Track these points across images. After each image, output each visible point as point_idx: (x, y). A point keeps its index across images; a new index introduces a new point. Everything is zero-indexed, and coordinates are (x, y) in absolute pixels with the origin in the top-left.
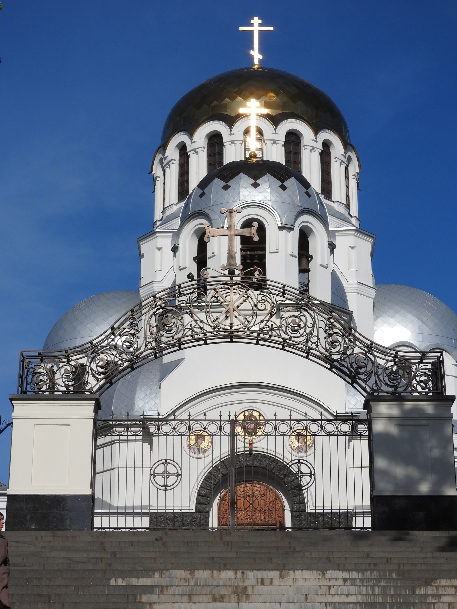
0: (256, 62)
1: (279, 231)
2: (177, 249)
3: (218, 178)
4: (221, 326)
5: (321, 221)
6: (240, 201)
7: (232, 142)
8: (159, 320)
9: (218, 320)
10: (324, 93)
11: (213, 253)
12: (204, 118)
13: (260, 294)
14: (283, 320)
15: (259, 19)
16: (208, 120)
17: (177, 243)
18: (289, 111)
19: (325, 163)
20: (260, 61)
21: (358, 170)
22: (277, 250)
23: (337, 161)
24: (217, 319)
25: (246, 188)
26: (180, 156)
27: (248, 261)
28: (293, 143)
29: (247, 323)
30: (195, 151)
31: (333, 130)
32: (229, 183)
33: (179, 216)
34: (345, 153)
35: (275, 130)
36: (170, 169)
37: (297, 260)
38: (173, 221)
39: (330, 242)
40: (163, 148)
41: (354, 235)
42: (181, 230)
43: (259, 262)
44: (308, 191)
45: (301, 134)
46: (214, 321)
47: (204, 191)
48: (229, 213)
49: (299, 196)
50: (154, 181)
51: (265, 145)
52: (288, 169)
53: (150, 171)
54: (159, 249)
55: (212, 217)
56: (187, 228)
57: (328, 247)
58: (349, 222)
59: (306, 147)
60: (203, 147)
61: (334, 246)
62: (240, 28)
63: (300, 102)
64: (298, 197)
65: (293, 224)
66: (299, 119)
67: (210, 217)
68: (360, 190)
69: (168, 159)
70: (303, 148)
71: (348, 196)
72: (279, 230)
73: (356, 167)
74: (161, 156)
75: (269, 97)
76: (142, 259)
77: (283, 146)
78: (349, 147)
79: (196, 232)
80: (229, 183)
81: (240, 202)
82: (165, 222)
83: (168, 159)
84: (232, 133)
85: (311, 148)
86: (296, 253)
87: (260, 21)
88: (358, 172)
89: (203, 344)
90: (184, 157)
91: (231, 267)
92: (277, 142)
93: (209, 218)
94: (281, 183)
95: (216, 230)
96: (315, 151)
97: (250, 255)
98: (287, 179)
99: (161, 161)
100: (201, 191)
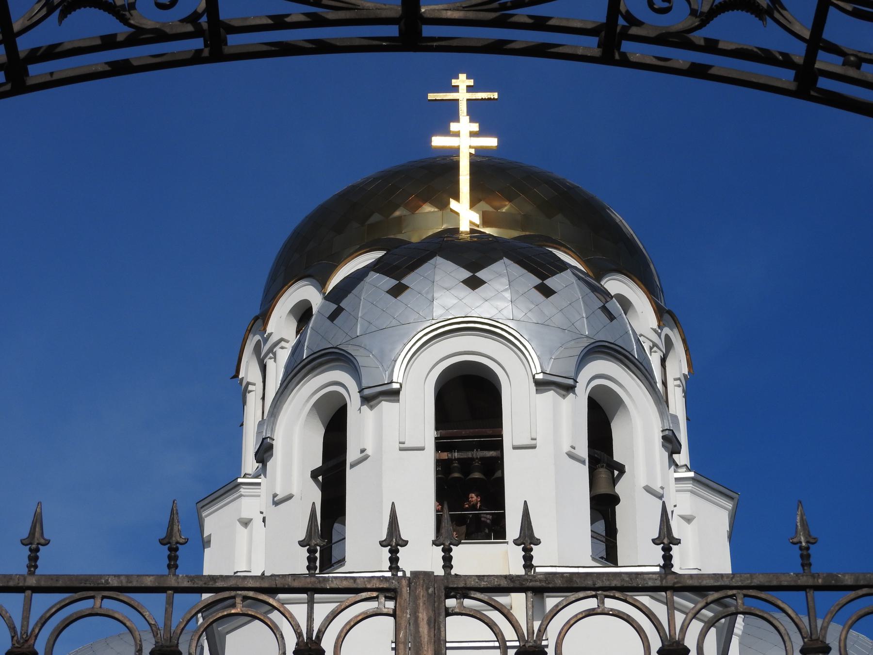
1: (536, 393)
5: (643, 378)
11: (363, 451)
18: (537, 234)
22: (532, 439)
25: (448, 289)
27: (456, 475)
32: (405, 281)
34: (659, 326)
36: (275, 361)
37: (585, 470)
39: (667, 433)
41: (692, 492)
42: (280, 402)
43: (484, 477)
49: (586, 312)
50: (243, 393)
53: (234, 373)
54: (246, 523)
55: (361, 361)
57: (663, 446)
65: (572, 375)
66: (559, 247)
67: (355, 362)
68: (689, 420)
69: (274, 339)
72: (538, 391)
74: (258, 337)
76: (205, 550)
78: (667, 317)
79: (319, 406)
80: (405, 281)
83: (274, 339)
86: (583, 451)
87: (471, 82)
89: (196, 59)
94: (538, 281)
97: (459, 460)
98: (554, 274)
99: (257, 349)
100: (334, 307)
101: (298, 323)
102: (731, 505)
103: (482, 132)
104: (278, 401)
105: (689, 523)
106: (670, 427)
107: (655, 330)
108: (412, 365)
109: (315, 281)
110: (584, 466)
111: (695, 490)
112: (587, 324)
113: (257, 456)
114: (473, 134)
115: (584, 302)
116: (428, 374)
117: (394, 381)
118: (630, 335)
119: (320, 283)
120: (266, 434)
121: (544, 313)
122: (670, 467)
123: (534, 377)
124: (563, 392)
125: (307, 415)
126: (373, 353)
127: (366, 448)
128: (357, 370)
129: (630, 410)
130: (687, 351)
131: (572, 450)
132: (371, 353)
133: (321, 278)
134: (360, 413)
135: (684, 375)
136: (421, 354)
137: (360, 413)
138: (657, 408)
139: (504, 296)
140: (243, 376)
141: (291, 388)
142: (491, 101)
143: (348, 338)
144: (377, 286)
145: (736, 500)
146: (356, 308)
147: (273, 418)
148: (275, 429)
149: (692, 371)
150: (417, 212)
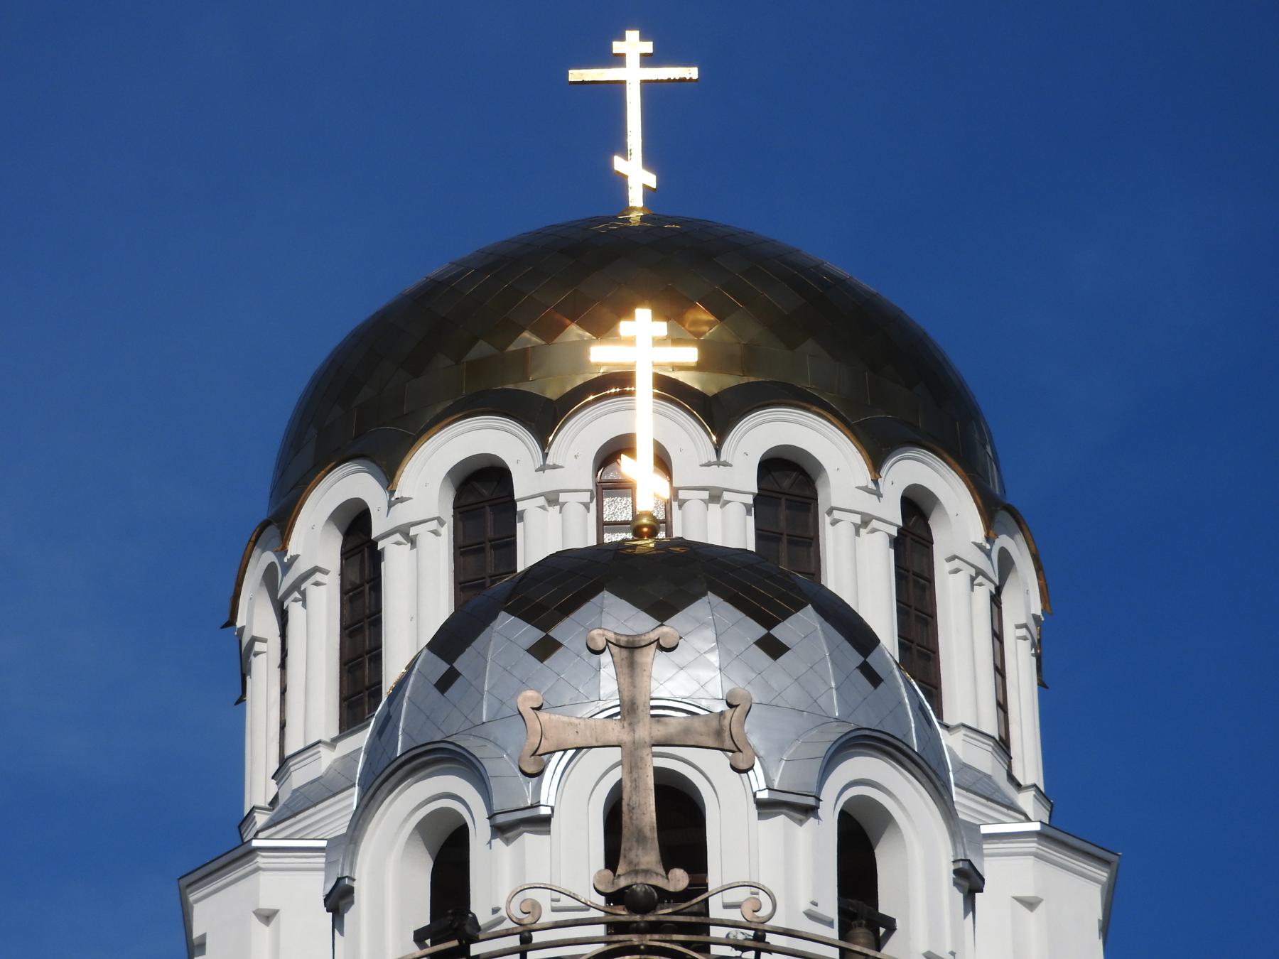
0: (636, 199)
1: (759, 819)
3: (511, 611)
5: (924, 780)
6: (601, 703)
7: (552, 497)
10: (902, 311)
11: (495, 911)
12: (439, 409)
15: (643, 38)
16: (452, 415)
17: (346, 874)
19: (911, 577)
20: (648, 192)
21: (1037, 608)
23: (956, 571)
26: (347, 554)
30: (406, 535)
31: (940, 450)
34: (988, 539)
35: (718, 452)
36: (304, 605)
39: (961, 865)
40: (279, 527)
41: (1036, 855)
42: (364, 821)
44: (867, 660)
45: (819, 467)
48: (625, 653)
49: (836, 683)
51: (680, 507)
53: (226, 618)
54: (267, 917)
57: (955, 884)
58: (1012, 807)
59: (836, 514)
61: (979, 880)
62: (570, 71)
63: (809, 346)
64: (833, 685)
65: (814, 790)
66: (809, 406)
67: (482, 770)
69: (301, 567)
70: (825, 521)
71: (1002, 706)
72: (761, 816)
74: (269, 557)
75: (690, 326)
77: (748, 513)
78: (1003, 516)
80: (556, 633)
81: (602, 705)
82: (289, 814)
87: (648, 47)
91: (640, 879)
92: (726, 496)
93: (479, 771)
95: (571, 724)
96: (874, 531)
98: (785, 615)
99: (270, 579)
100: (445, 667)
101: (344, 537)
102: (1106, 875)
103: (675, 340)
104: (358, 820)
106: (965, 855)
107: (980, 547)
109: (374, 466)
110: (830, 929)
111: (1043, 853)
112: (837, 697)
113: (328, 902)
114: (658, 342)
117: (542, 803)
119: (383, 471)
120: (343, 869)
121: (770, 685)
122: (966, 915)
123: (755, 795)
125: (407, 842)
126: (509, 752)
127: (500, 906)
128: (485, 783)
129: (901, 826)
130: (1039, 569)
131: (814, 908)
132: (506, 752)
133: (385, 463)
134: (491, 848)
135: (1035, 617)
137: (491, 848)
139: (708, 660)
140: (245, 624)
141: (381, 799)
142: (686, 83)
143: (468, 725)
144: (512, 639)
145: (1114, 866)
146: (480, 674)
147: (352, 846)
149: (1048, 608)
150: (554, 342)
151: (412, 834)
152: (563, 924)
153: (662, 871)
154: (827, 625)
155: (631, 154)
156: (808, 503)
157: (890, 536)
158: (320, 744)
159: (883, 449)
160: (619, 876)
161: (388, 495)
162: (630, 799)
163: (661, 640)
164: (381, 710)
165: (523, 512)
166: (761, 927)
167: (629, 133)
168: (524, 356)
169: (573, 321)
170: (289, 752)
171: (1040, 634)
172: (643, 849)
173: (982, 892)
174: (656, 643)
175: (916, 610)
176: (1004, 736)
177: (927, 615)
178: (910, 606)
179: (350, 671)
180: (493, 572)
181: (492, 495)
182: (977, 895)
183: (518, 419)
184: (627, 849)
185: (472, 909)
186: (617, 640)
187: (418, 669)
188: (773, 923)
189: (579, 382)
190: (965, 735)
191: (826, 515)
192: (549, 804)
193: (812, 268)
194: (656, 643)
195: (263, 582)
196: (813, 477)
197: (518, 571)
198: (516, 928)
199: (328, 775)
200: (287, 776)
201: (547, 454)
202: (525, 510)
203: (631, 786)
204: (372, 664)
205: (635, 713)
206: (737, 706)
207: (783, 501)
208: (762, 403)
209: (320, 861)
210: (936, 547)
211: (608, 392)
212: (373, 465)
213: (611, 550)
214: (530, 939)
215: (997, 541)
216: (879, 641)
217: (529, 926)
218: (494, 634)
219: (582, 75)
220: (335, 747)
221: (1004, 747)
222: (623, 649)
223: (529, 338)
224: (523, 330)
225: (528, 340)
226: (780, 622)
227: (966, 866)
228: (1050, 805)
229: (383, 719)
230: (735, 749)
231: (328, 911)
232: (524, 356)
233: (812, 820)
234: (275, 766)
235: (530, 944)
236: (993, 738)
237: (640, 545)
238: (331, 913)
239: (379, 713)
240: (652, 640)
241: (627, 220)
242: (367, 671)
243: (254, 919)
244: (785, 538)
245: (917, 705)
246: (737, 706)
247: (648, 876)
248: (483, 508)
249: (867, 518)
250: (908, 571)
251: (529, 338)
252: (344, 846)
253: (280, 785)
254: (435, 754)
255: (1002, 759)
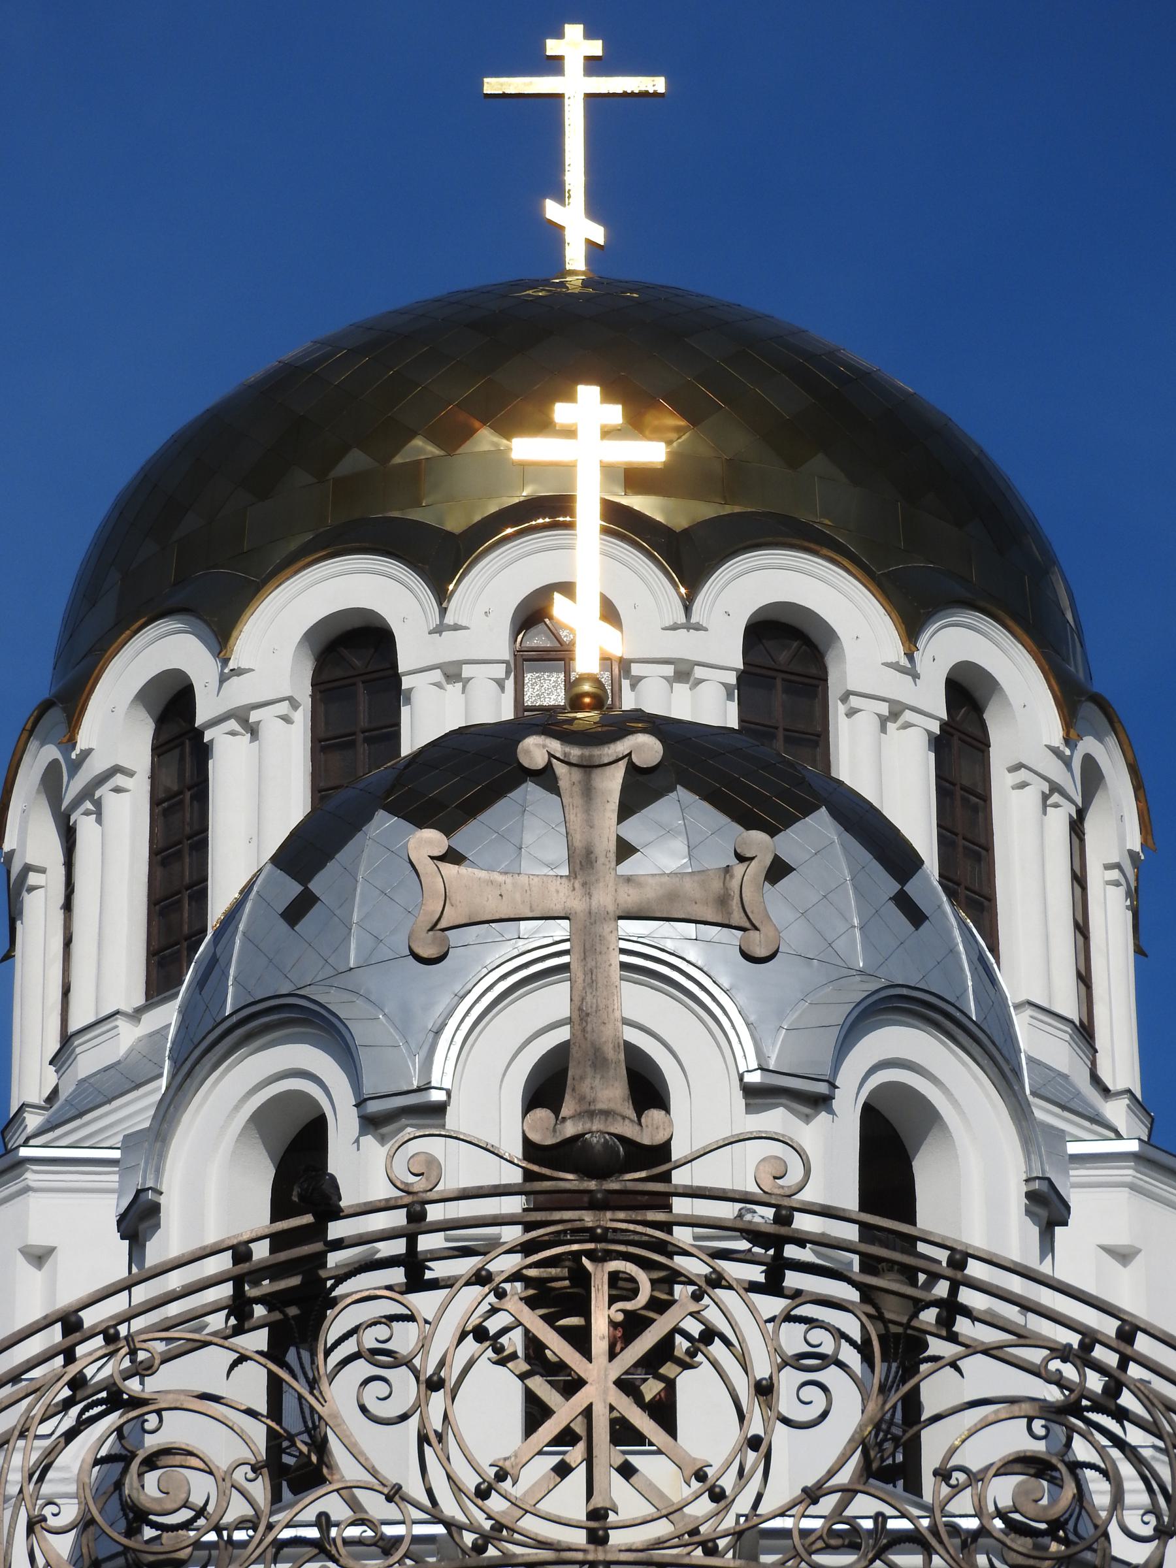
0: (575, 259)
2: (152, 1222)
3: (393, 810)
4: (530, 1524)
5: (985, 1061)
6: (521, 942)
7: (451, 671)
8: (101, 1491)
9: (507, 1485)
12: (293, 545)
13: (789, 1318)
14: (957, 1489)
15: (589, 35)
16: (316, 551)
17: (149, 1184)
19: (959, 793)
21: (1134, 841)
23: (1022, 785)
24: (501, 1476)
28: (783, 680)
29: (704, 1505)
31: (1001, 613)
33: (160, 1075)
34: (1067, 741)
35: (688, 609)
36: (99, 821)
38: (116, 1103)
39: (1036, 1185)
40: (65, 710)
41: (1133, 1187)
45: (831, 635)
46: (482, 1493)
47: (310, 886)
48: (577, 774)
51: (633, 687)
52: (796, 770)
55: (360, 1032)
56: (211, 1098)
57: (1028, 1212)
59: (854, 701)
60: (290, 699)
62: (486, 80)
63: (819, 463)
64: (856, 922)
65: (826, 1071)
70: (837, 710)
71: (1084, 979)
73: (1126, 818)
74: (51, 752)
77: (730, 697)
78: (1089, 710)
79: (262, 1120)
82: (73, 1112)
84: (446, 621)
85: (884, 709)
87: (596, 48)
88: (1137, 848)
90: (182, 759)
91: (597, 1125)
92: (699, 672)
96: (907, 725)
99: (52, 783)
100: (296, 889)
103: (635, 425)
104: (169, 1105)
105: (1125, 1265)
106: (1043, 1171)
107: (1056, 752)
108: (473, 1045)
114: (608, 433)
115: (855, 888)
116: (504, 1075)
118: (958, 954)
119: (213, 630)
120: (144, 1179)
124: (807, 1110)
126: (386, 1011)
134: (358, 1149)
135: (1132, 854)
136: (491, 1020)
137: (358, 1149)
138: (1017, 1128)
140: (14, 847)
146: (347, 900)
147: (158, 1145)
148: (164, 1170)
149: (1150, 842)
150: (458, 452)
151: (245, 1128)
152: (475, 1192)
153: (631, 1113)
154: (848, 837)
155: (569, 197)
156: (811, 685)
157: (929, 733)
158: (117, 1016)
159: (922, 611)
160: (564, 1119)
161: (219, 665)
162: (583, 999)
163: (633, 756)
164: (203, 952)
165: (410, 690)
166: (786, 1202)
167: (567, 168)
168: (415, 471)
169: (484, 423)
170: (74, 1026)
171: (1137, 880)
172: (602, 1077)
173: (1067, 1225)
174: (626, 760)
175: (964, 839)
176: (1085, 1021)
177: (980, 846)
178: (956, 834)
179: (163, 913)
180: (366, 724)
181: (366, 667)
182: (1058, 1230)
183: (405, 560)
184: (577, 1077)
185: (331, 1169)
186: (565, 754)
187: (258, 892)
188: (808, 1195)
189: (493, 508)
190: (1032, 1017)
191: (839, 701)
192: (444, 1086)
193: (823, 355)
194: (626, 760)
195: (42, 787)
196: (821, 647)
197: (403, 755)
198: (401, 1197)
199: (128, 1059)
200: (69, 1062)
201: (446, 609)
202: (413, 688)
203: (584, 980)
204: (194, 904)
205: (592, 867)
206: (752, 859)
207: (779, 683)
208: (749, 543)
209: (112, 1178)
210: (994, 752)
211: (534, 523)
212: (198, 621)
213: (538, 725)
214: (423, 1215)
215: (1081, 744)
216: (922, 862)
217: (421, 1194)
218: (369, 842)
219: (502, 85)
220: (139, 1021)
221: (1087, 1037)
222: (574, 770)
223: (422, 447)
224: (413, 434)
225: (420, 450)
226: (781, 831)
227: (1045, 1184)
228: (1150, 1120)
229: (207, 961)
230: (747, 925)
231: (122, 1238)
232: (415, 471)
233: (823, 1115)
234: (54, 1046)
235: (423, 1224)
236: (1071, 1022)
237: (580, 719)
238: (127, 1242)
239: (201, 955)
240: (621, 756)
241: (563, 284)
242: (186, 915)
243: (20, 1258)
244: (780, 734)
245: (975, 958)
246: (752, 859)
247: (610, 1119)
248: (354, 684)
249: (897, 709)
250: (954, 785)
251: (422, 447)
252: (146, 1145)
253: (60, 1073)
254: (279, 1013)
255: (1085, 1054)
